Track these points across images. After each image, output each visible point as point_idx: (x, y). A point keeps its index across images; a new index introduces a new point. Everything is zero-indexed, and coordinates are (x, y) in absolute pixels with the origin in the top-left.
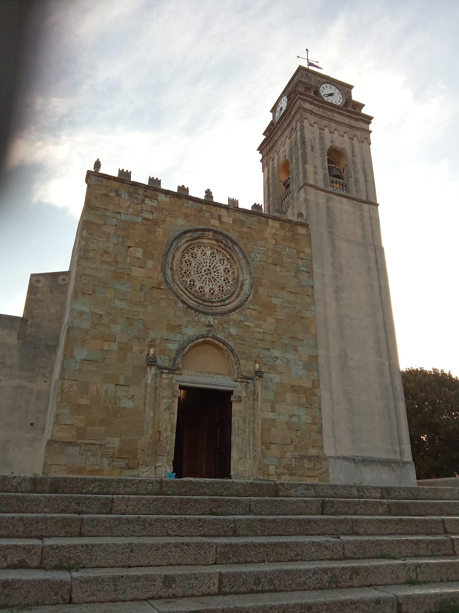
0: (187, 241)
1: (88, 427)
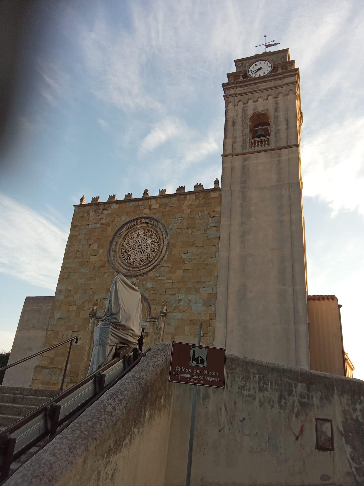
0: (126, 230)
1: (56, 358)
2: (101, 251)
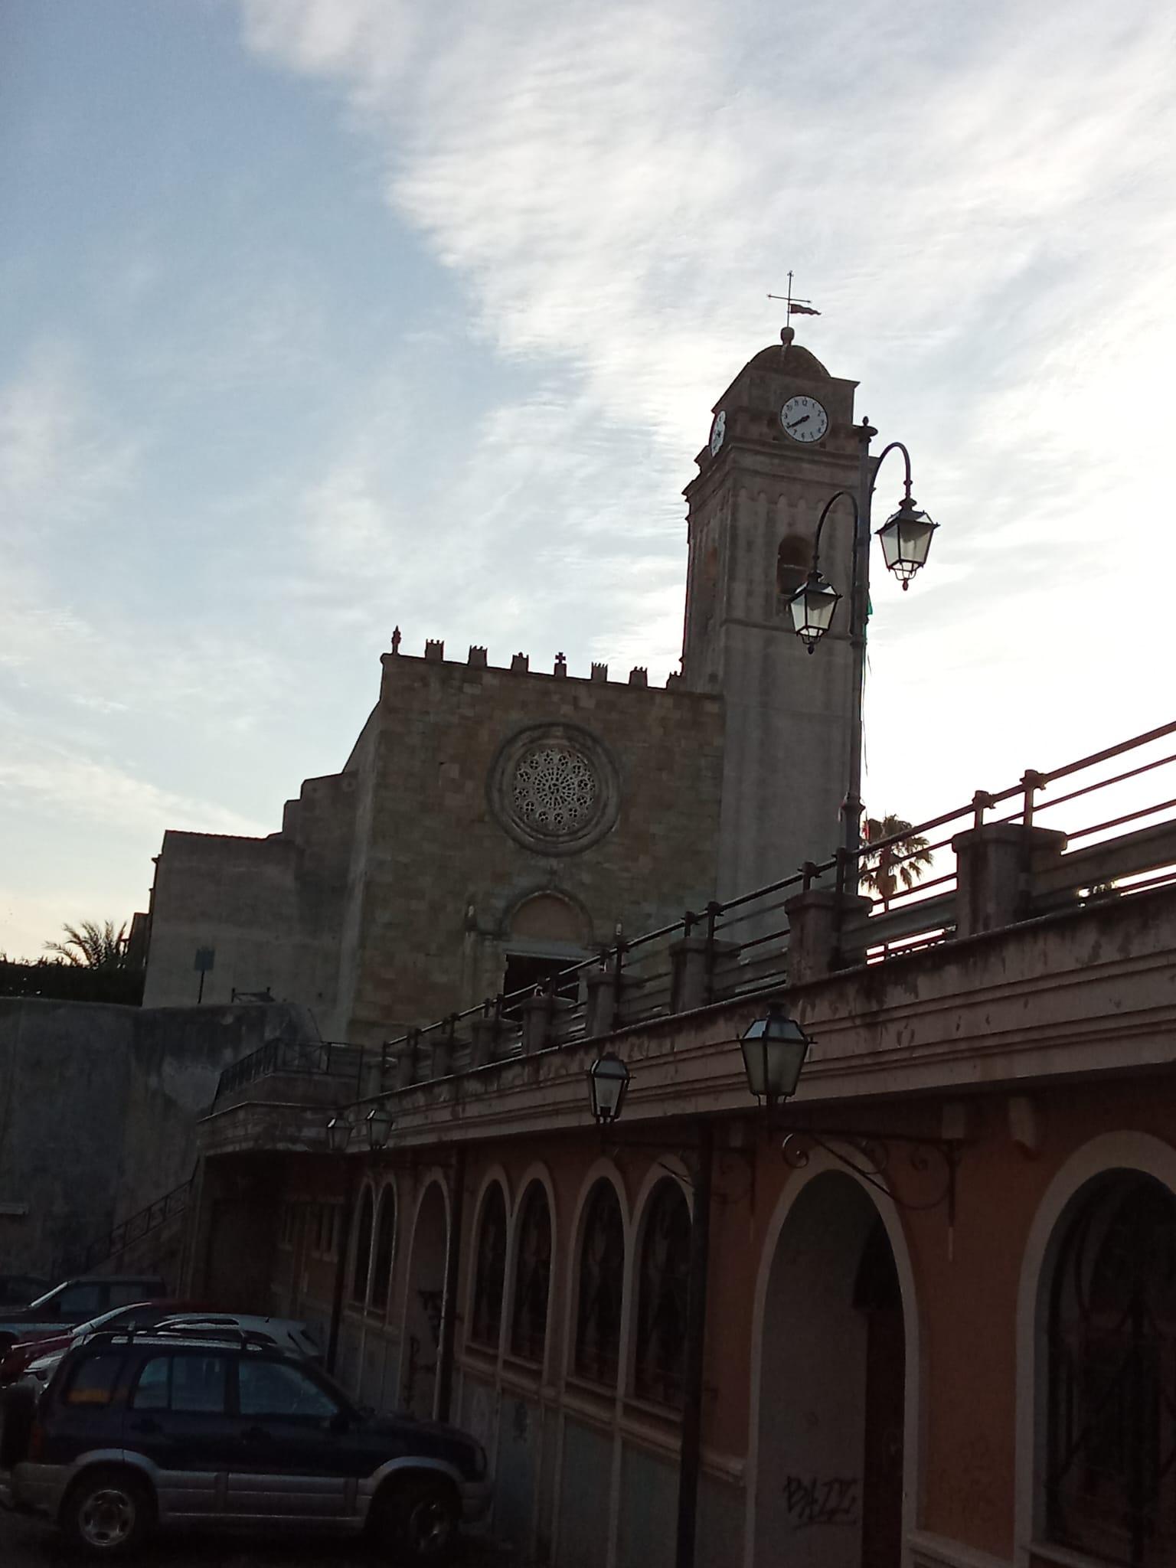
2: (470, 785)
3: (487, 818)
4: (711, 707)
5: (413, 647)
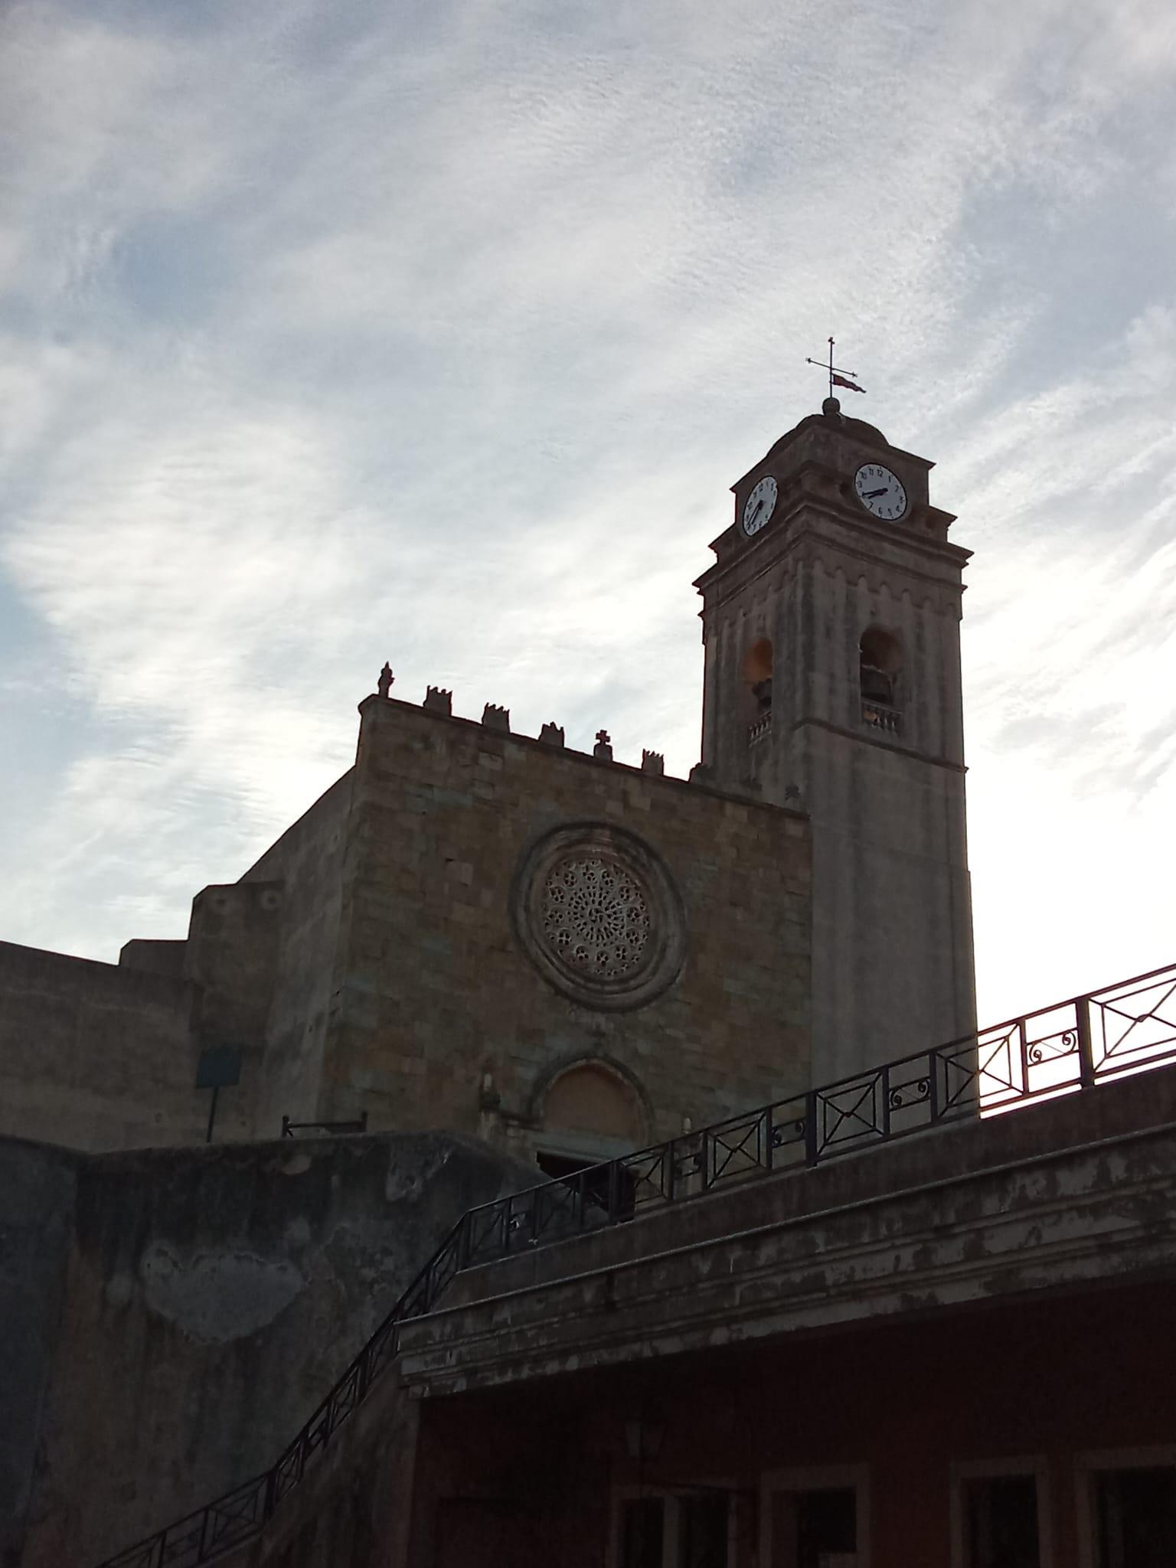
2: (487, 897)
3: (511, 947)
4: (793, 829)
5: (409, 690)
